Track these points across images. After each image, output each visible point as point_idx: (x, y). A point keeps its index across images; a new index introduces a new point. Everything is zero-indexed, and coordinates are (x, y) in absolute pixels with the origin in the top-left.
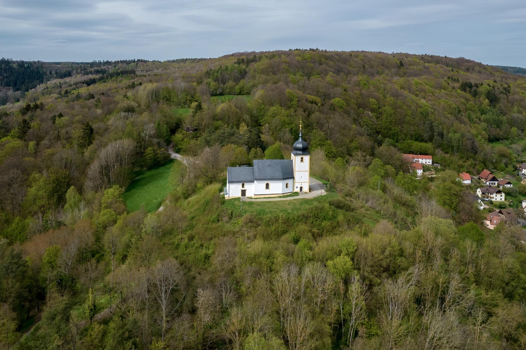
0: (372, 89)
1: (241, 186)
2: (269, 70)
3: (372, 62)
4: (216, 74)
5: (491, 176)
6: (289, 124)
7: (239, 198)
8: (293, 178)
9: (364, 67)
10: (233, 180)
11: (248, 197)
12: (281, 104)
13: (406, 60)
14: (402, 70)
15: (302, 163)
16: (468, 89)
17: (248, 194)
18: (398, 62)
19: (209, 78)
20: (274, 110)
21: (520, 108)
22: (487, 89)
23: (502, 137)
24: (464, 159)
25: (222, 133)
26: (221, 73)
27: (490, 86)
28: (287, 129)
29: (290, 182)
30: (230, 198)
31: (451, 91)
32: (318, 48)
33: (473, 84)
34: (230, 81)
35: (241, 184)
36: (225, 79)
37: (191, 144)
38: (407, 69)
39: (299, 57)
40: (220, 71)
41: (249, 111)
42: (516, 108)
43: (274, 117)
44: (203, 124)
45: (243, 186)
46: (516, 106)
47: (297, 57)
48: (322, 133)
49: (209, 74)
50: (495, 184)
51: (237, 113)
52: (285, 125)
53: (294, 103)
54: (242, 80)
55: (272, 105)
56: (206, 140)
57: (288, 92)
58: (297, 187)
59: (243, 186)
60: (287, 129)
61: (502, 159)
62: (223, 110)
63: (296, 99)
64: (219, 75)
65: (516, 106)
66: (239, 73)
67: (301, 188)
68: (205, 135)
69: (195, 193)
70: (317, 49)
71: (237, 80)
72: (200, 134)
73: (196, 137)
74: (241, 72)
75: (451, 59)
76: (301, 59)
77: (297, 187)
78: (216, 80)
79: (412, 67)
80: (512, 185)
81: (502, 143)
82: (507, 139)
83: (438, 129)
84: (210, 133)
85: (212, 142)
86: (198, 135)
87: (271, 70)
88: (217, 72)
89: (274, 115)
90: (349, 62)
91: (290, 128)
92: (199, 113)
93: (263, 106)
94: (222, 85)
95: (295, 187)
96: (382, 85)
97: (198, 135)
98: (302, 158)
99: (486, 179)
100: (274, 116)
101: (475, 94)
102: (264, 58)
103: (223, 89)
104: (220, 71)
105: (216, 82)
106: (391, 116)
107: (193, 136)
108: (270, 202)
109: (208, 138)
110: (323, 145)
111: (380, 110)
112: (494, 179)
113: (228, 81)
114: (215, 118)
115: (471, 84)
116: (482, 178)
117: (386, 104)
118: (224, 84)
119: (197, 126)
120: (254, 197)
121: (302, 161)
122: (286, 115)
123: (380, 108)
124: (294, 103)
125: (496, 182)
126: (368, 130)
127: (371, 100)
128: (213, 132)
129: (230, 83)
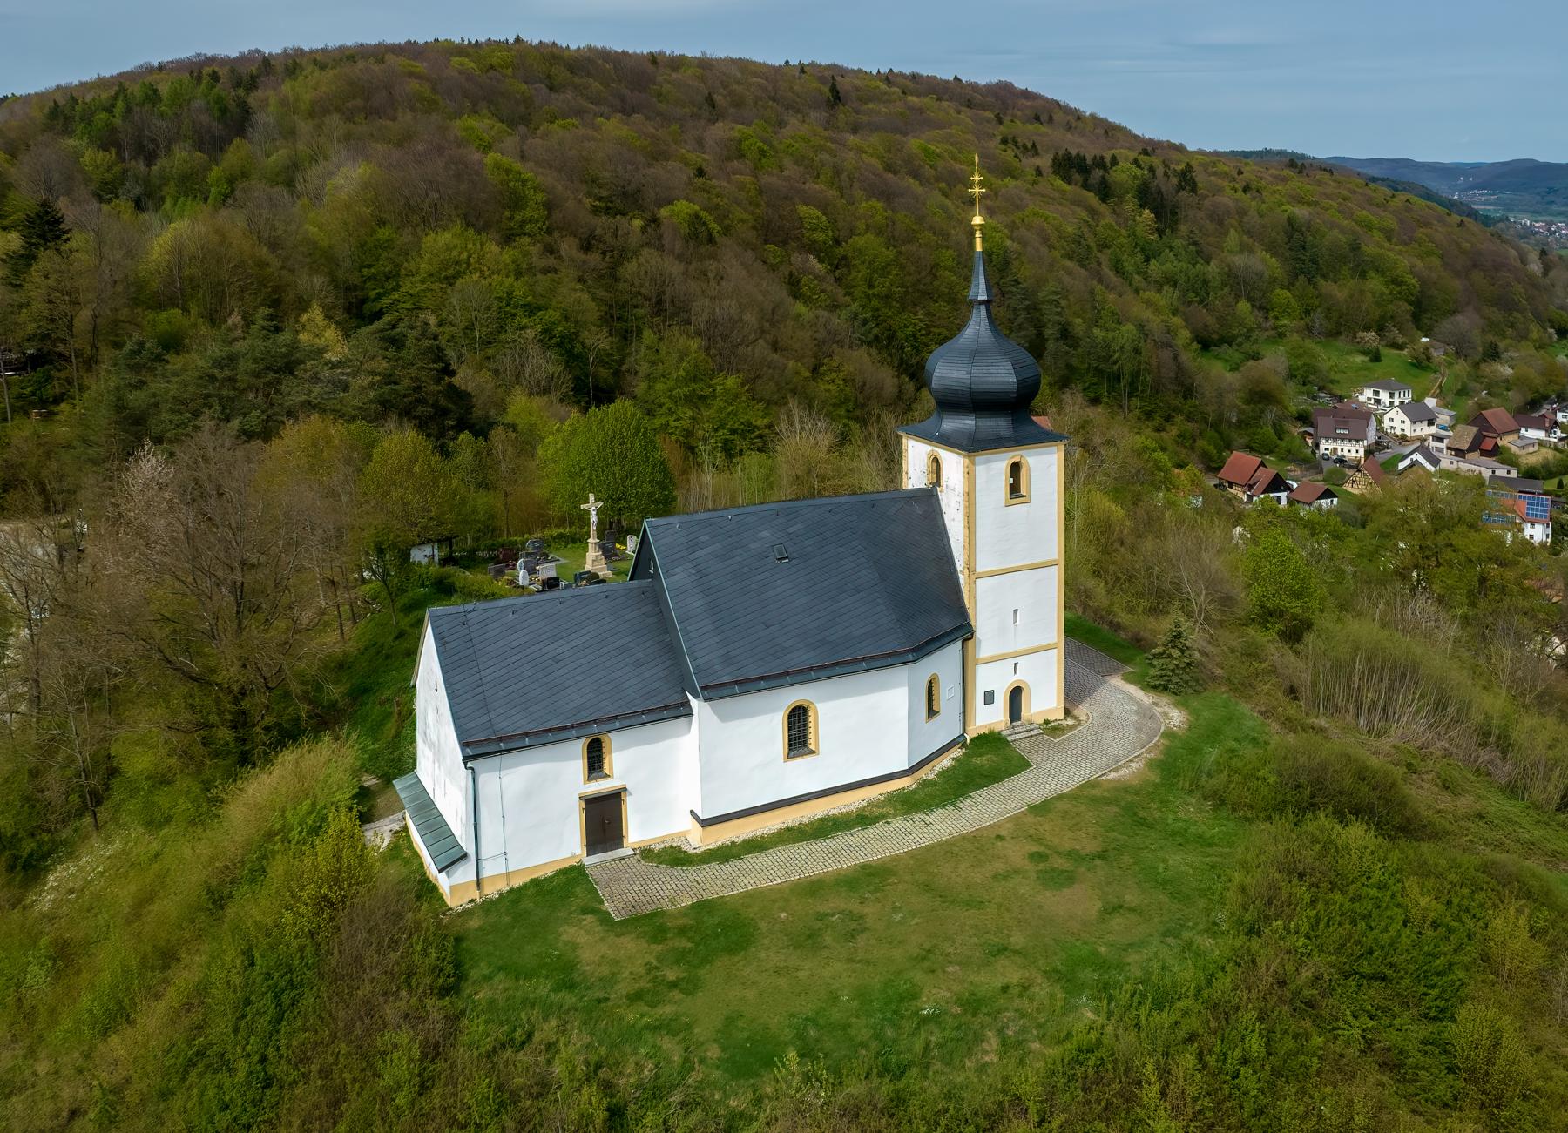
0: (791, 170)
1: (579, 765)
2: (350, 105)
3: (735, 87)
4: (103, 115)
5: (1265, 476)
6: (531, 310)
7: (573, 876)
8: (962, 630)
9: (710, 100)
10: (506, 726)
11: (646, 853)
12: (476, 220)
13: (843, 84)
14: (843, 115)
15: (1019, 510)
16: (1077, 177)
17: (638, 830)
18: (826, 89)
19: (67, 132)
20: (449, 248)
21: (1245, 238)
22: (1135, 177)
23: (1215, 336)
24: (1158, 420)
25: (218, 364)
26: (129, 110)
27: (1139, 166)
28: (530, 334)
29: (944, 663)
30: (491, 891)
31: (1034, 183)
32: (524, 37)
33: (1089, 161)
34: (176, 148)
35: (579, 747)
36: (153, 141)
37: (15, 441)
38: (857, 112)
39: (465, 60)
40: (120, 104)
41: (323, 259)
42: (1233, 237)
43: (450, 280)
44: (84, 317)
45: (595, 763)
46: (1232, 231)
47: (456, 60)
48: (694, 344)
49: (68, 120)
50: (1279, 499)
51: (262, 264)
52: (514, 316)
53: (528, 213)
54: (237, 141)
55: (429, 219)
56: (120, 407)
57: (498, 166)
58: (989, 697)
59: (595, 763)
60: (530, 334)
61: (1262, 411)
62: (177, 249)
63: (540, 197)
64: (118, 121)
65: (1232, 231)
66: (217, 114)
67: (1016, 694)
68: (103, 383)
69: (104, 813)
70: (518, 40)
71: (213, 145)
72: (69, 382)
73: (43, 403)
74: (224, 111)
75: (974, 87)
76: (472, 65)
77: (989, 697)
78: (108, 140)
79: (871, 106)
80: (1335, 500)
81: (1217, 357)
82: (1229, 341)
83: (1060, 314)
84: (136, 368)
85: (165, 416)
86: (55, 388)
87: (359, 102)
88: (109, 109)
89: (450, 272)
90: (655, 84)
91: (539, 328)
92: (46, 259)
93: (384, 234)
94: (140, 166)
95: (980, 698)
96: (825, 156)
97: (55, 388)
98: (1015, 469)
99: (1251, 487)
100: (450, 274)
101: (1105, 192)
102: (310, 68)
103: (146, 182)
104: (120, 104)
105: (106, 149)
106: (884, 271)
107: (19, 397)
108: (871, 876)
109: (136, 398)
110: (702, 398)
111: (841, 251)
112: (1277, 484)
113: (168, 148)
114: (147, 298)
115: (1084, 159)
116: (1231, 484)
117: (861, 225)
118: (150, 158)
119: (45, 337)
120: (697, 840)
121: (1014, 490)
122: (512, 267)
123: (837, 242)
124: (528, 213)
125: (1283, 495)
126: (865, 322)
127: (803, 210)
128: (159, 358)
129: (182, 157)
